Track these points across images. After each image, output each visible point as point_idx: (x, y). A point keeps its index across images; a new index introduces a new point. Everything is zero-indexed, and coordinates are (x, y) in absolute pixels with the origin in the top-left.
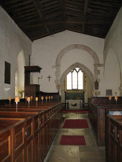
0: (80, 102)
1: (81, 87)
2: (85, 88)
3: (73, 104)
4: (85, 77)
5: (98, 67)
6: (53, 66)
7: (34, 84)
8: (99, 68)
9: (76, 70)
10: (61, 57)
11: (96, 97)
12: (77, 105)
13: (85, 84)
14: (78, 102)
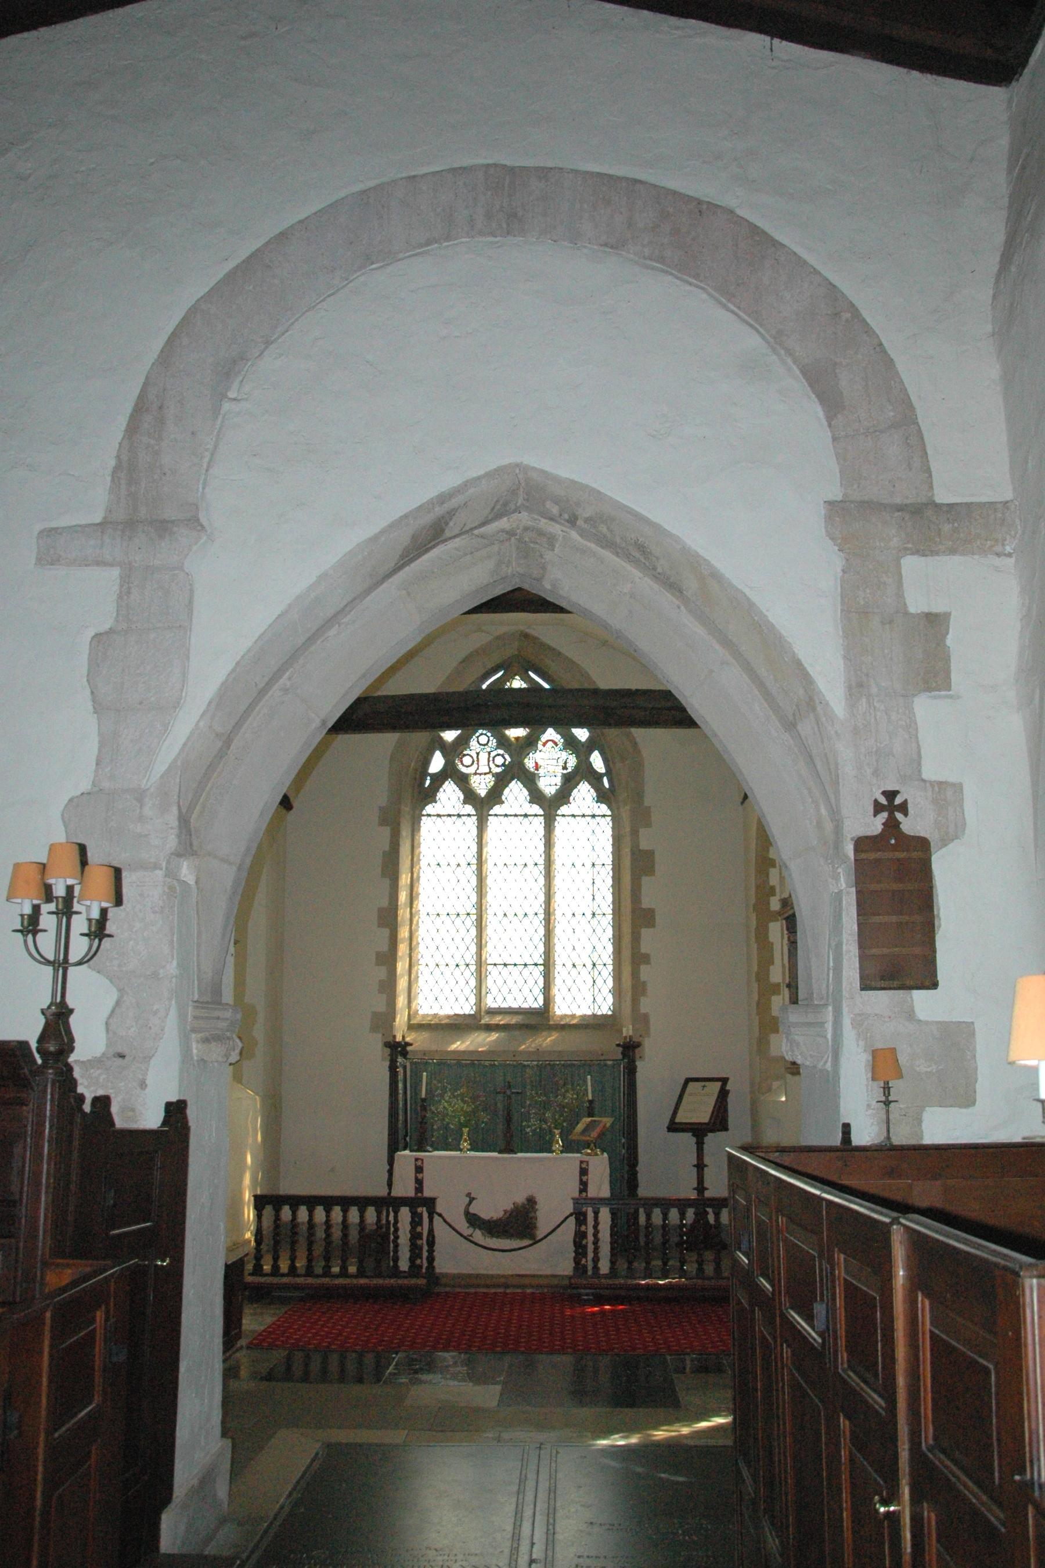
0: (584, 1186)
1: (585, 992)
2: (635, 1002)
3: (491, 1209)
4: (633, 865)
5: (910, 564)
6: (51, 533)
7: (927, 1140)
8: (928, 581)
9: (530, 780)
10: (228, 370)
11: (900, 1138)
12: (544, 1223)
14: (552, 1179)
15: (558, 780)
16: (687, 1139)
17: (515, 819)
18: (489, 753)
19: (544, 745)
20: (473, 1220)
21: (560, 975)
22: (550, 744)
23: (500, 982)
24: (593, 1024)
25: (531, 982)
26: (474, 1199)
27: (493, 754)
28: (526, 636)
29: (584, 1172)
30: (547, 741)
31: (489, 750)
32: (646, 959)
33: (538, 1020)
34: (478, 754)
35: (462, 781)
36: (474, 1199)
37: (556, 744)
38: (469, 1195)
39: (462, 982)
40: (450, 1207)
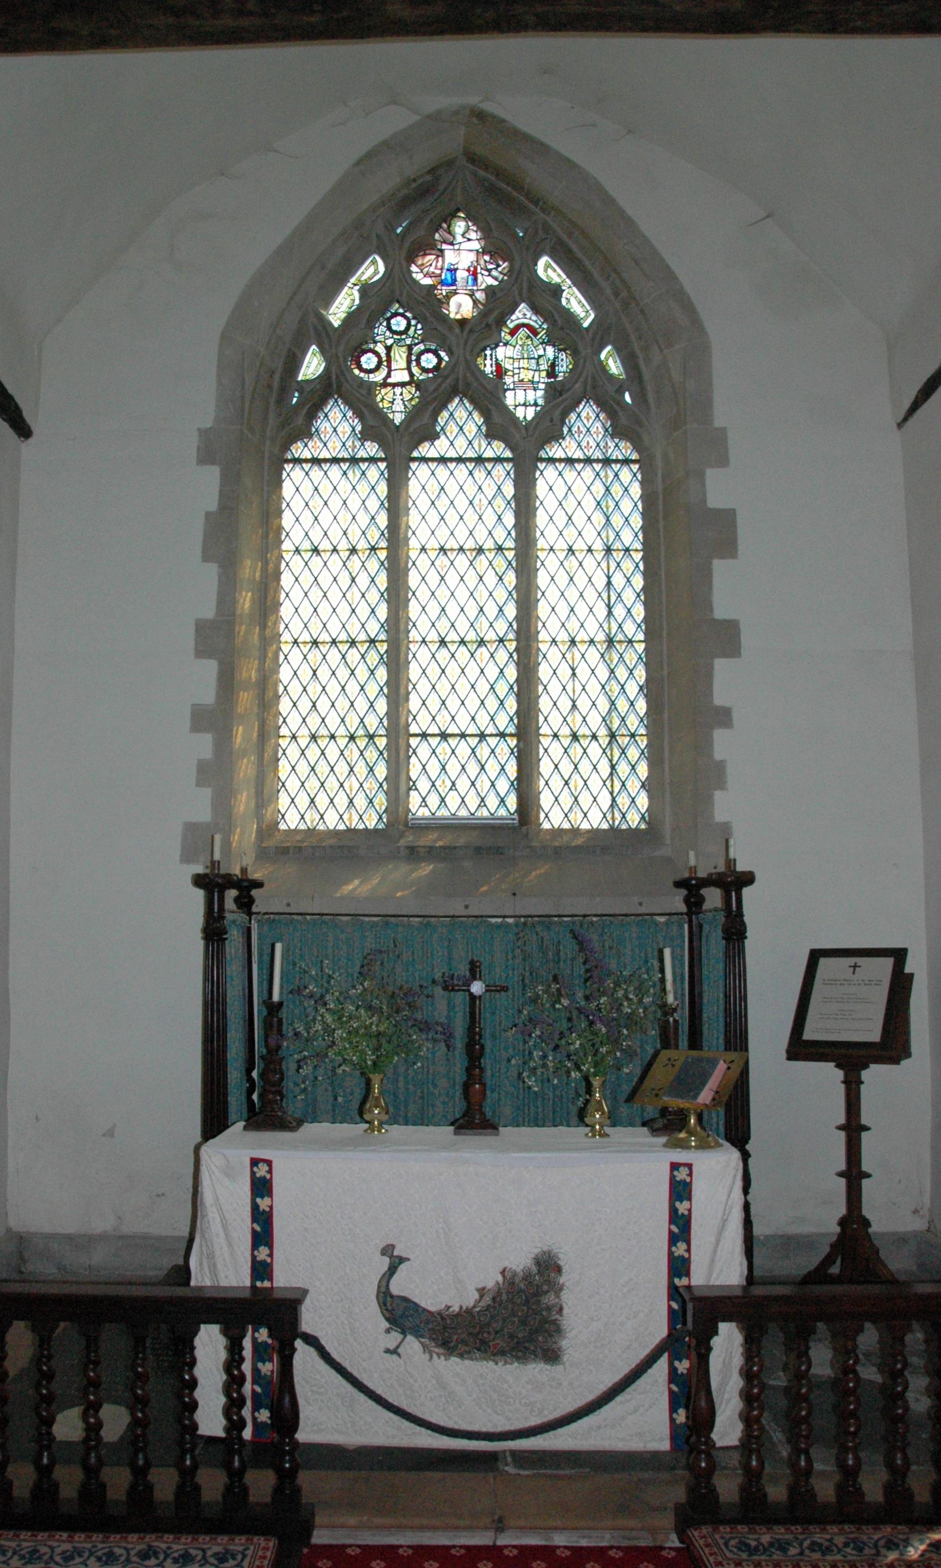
3: (449, 1282)
9: (487, 397)
14: (604, 1223)
15: (538, 396)
16: (828, 1075)
17: (456, 494)
18: (410, 348)
19: (513, 333)
20: (400, 1314)
21: (551, 758)
22: (523, 332)
23: (434, 768)
24: (609, 844)
25: (492, 768)
26: (402, 1260)
27: (416, 349)
28: (481, 115)
29: (680, 1190)
30: (518, 327)
31: (408, 342)
33: (512, 840)
34: (389, 349)
35: (362, 402)
36: (402, 1260)
37: (534, 332)
38: (387, 1250)
39: (361, 770)
40: (339, 1314)
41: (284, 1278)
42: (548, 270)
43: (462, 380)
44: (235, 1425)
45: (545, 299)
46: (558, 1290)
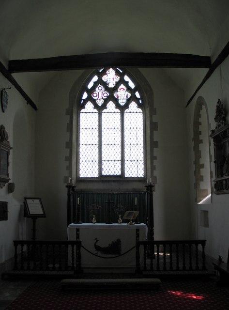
3: (104, 243)
13: (155, 155)
20: (98, 248)
21: (127, 164)
22: (122, 89)
32: (155, 158)
33: (120, 179)
35: (94, 102)
38: (96, 239)
41: (81, 240)
42: (126, 78)
43: (111, 97)
44: (73, 264)
45: (126, 84)
46: (120, 244)
